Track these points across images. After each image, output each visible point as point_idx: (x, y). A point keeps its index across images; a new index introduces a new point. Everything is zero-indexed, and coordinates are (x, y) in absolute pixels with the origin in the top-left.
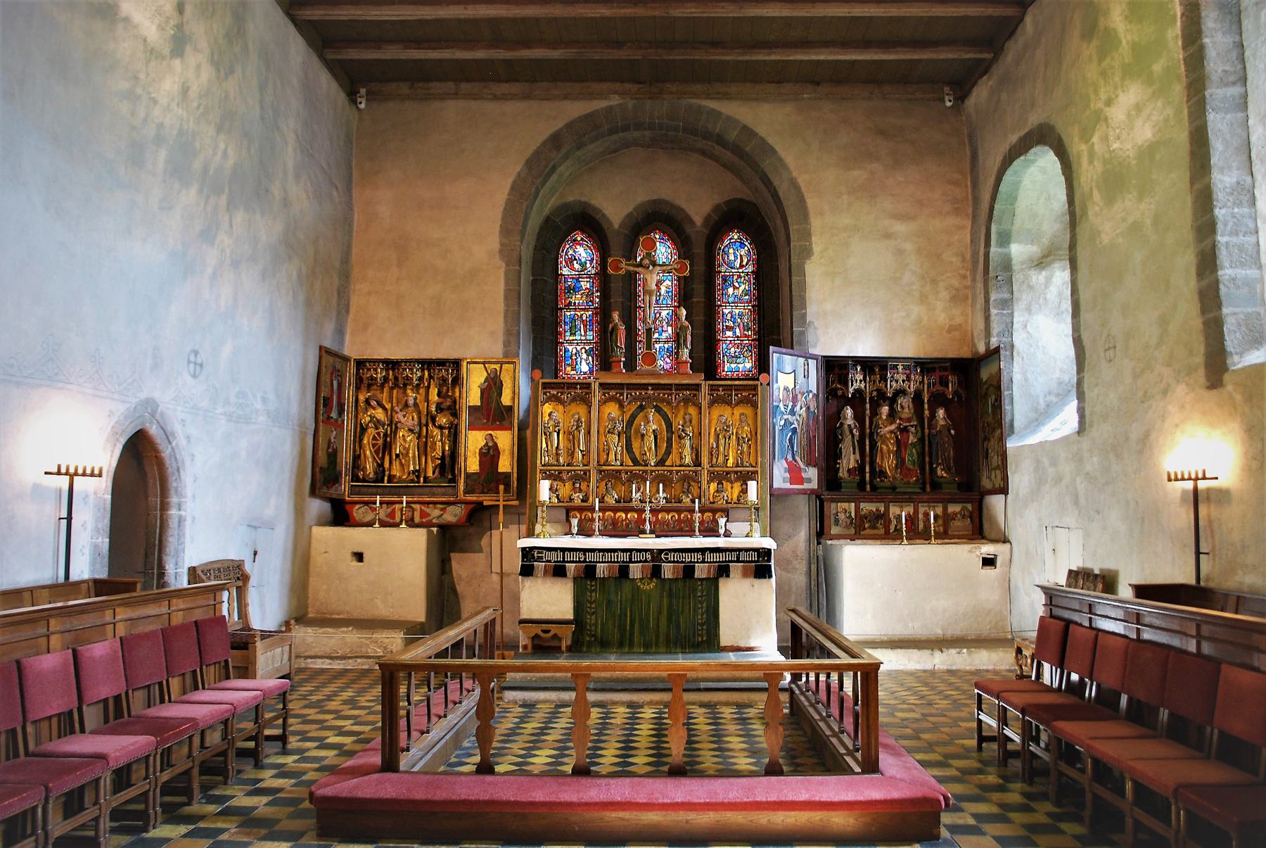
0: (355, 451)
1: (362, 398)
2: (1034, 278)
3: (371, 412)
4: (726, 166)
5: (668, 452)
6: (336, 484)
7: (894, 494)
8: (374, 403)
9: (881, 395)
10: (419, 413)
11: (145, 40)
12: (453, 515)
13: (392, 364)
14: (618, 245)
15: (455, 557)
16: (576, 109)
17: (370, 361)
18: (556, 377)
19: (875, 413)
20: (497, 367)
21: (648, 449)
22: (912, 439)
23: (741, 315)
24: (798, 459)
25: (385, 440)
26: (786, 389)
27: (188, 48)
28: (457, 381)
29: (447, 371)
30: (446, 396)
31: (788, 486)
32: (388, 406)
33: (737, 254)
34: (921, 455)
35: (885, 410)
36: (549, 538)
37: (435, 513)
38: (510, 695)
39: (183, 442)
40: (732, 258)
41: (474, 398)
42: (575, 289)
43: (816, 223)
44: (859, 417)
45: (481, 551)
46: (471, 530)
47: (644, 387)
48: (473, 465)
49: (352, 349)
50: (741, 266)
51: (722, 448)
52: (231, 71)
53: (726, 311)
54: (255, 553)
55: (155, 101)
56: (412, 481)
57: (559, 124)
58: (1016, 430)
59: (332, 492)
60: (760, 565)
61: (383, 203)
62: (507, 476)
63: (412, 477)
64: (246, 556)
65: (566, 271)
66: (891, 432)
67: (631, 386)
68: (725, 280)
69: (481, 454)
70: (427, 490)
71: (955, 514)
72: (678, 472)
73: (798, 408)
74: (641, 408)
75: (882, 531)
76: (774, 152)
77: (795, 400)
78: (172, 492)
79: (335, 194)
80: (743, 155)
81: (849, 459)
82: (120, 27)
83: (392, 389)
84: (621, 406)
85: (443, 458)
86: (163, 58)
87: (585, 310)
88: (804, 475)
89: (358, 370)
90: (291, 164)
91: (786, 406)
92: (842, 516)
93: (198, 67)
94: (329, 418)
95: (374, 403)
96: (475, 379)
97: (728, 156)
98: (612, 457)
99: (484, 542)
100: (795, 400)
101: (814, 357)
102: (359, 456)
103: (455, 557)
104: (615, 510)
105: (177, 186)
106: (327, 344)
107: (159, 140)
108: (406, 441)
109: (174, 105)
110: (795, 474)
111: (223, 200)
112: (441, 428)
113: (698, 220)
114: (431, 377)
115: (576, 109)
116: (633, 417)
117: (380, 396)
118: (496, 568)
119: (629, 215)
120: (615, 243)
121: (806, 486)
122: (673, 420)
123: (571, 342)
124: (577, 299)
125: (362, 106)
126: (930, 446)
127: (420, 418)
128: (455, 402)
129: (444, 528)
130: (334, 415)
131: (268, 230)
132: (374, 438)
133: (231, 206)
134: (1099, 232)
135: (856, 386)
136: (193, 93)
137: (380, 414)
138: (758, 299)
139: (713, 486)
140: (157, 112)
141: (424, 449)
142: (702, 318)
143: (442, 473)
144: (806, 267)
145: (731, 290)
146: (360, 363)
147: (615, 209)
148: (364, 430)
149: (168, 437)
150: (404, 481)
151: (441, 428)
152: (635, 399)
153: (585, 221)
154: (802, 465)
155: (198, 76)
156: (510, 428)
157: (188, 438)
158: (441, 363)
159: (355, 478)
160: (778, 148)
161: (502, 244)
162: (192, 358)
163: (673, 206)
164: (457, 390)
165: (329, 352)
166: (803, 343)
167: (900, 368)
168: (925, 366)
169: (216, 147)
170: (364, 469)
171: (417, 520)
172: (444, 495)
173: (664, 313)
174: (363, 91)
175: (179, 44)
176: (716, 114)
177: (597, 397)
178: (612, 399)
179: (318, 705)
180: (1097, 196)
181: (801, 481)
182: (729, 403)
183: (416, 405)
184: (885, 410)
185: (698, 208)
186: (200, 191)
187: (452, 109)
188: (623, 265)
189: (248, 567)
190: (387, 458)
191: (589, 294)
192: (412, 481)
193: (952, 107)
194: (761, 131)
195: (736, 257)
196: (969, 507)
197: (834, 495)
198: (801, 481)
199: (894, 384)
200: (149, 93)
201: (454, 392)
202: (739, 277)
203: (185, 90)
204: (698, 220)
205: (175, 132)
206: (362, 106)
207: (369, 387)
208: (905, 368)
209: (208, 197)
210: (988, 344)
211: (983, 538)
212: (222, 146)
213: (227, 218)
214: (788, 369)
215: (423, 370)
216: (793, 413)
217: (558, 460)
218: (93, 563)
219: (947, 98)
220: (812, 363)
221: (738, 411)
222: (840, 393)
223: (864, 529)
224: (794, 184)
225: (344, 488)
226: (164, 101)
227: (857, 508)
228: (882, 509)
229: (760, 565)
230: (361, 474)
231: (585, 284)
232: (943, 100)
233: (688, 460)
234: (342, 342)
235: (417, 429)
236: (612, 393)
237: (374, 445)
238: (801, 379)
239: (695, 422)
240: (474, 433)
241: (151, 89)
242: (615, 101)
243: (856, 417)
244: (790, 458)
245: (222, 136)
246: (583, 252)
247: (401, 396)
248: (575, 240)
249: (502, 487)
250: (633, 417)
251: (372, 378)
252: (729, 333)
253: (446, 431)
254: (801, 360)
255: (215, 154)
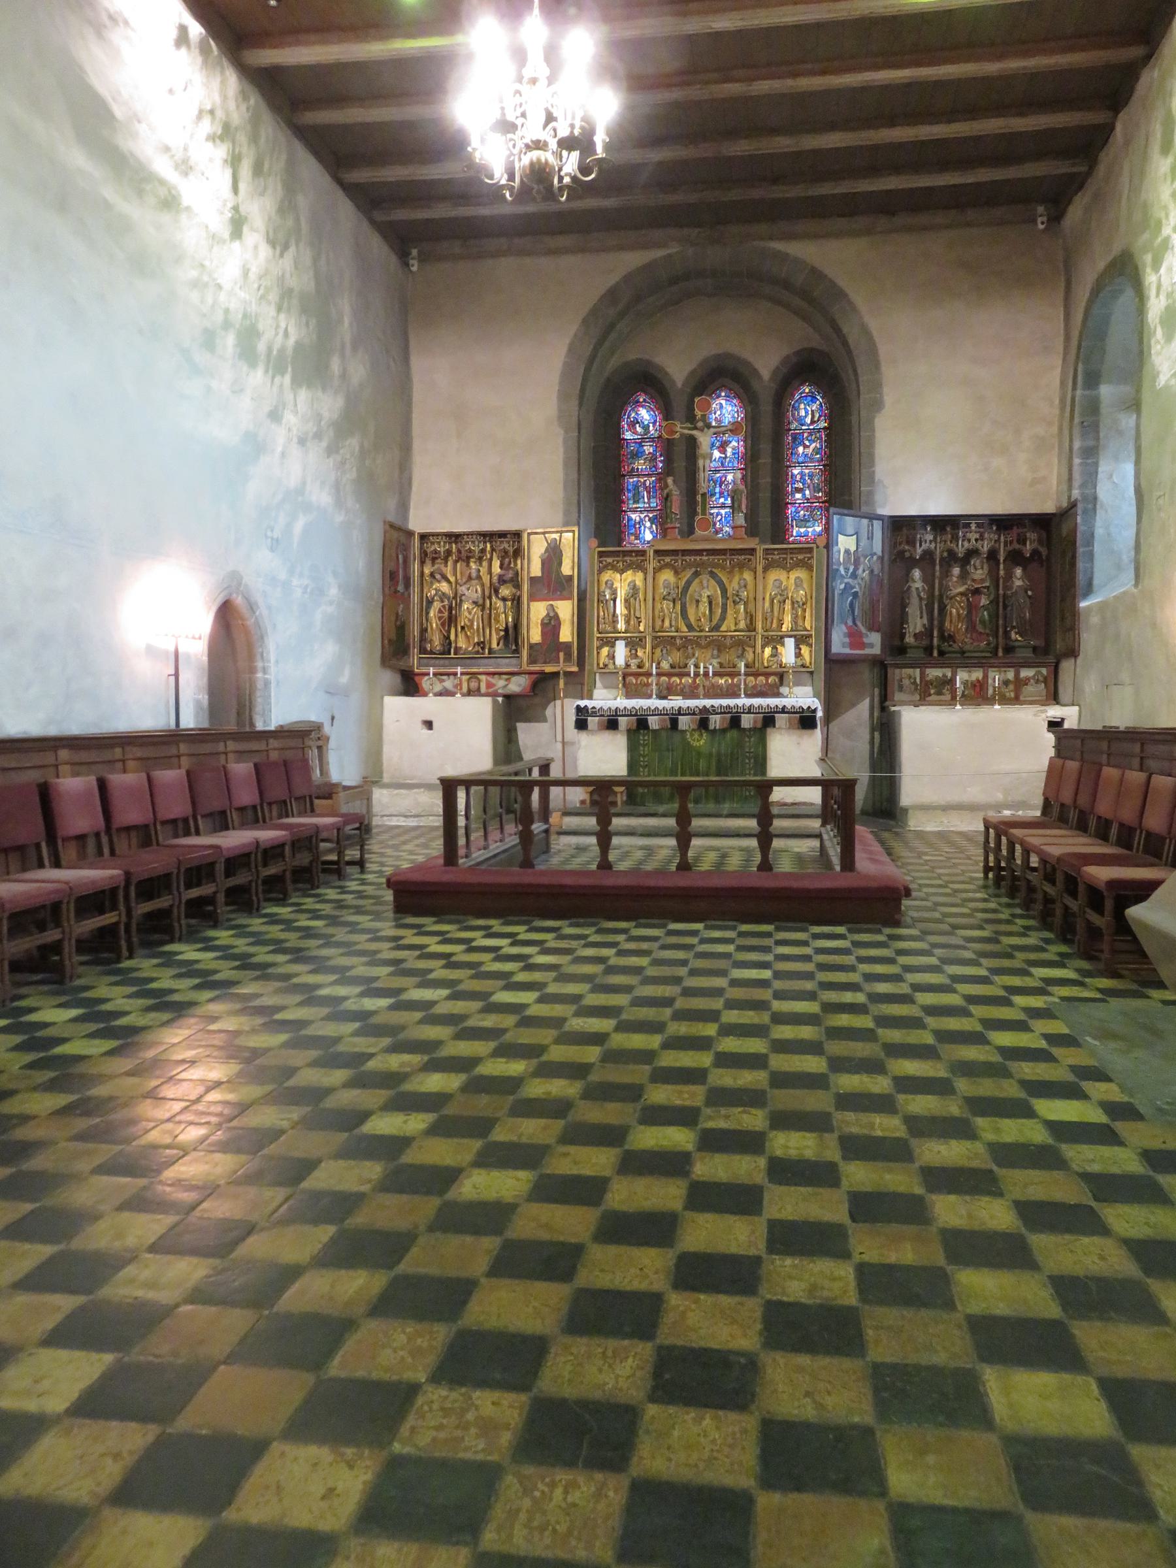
0: (422, 624)
1: (427, 571)
2: (1124, 423)
3: (436, 585)
4: (796, 312)
5: (723, 618)
6: (403, 654)
7: (966, 660)
8: (438, 576)
9: (952, 554)
10: (483, 585)
11: (207, 227)
12: (517, 685)
13: (455, 537)
14: (681, 405)
15: (520, 726)
16: (634, 259)
17: (433, 535)
18: (619, 545)
19: (946, 574)
20: (556, 536)
21: (699, 612)
22: (984, 601)
23: (811, 476)
24: (859, 624)
25: (450, 612)
26: (847, 552)
27: (245, 229)
28: (518, 553)
29: (510, 543)
30: (509, 568)
31: (847, 651)
32: (452, 579)
33: (808, 411)
34: (994, 616)
35: (956, 571)
36: (605, 698)
37: (500, 683)
38: (565, 840)
39: (265, 612)
40: (803, 413)
41: (536, 570)
42: (636, 455)
43: (889, 373)
44: (928, 579)
45: (545, 720)
46: (537, 700)
47: (699, 552)
48: (536, 636)
49: (418, 523)
50: (813, 422)
51: (776, 614)
52: (286, 247)
53: (796, 472)
54: (333, 718)
55: (219, 287)
56: (478, 653)
57: (613, 279)
58: (1095, 588)
59: (402, 664)
60: (806, 721)
61: (436, 372)
62: (567, 646)
63: (477, 648)
64: (324, 719)
65: (628, 435)
66: (962, 594)
67: (685, 552)
68: (794, 439)
69: (543, 624)
70: (493, 660)
71: (1028, 679)
72: (732, 637)
73: (860, 571)
74: (696, 574)
75: (948, 697)
76: (846, 295)
77: (857, 563)
78: (258, 657)
79: (392, 364)
80: (815, 300)
81: (916, 622)
82: (184, 217)
83: (456, 562)
84: (676, 573)
85: (506, 630)
86: (224, 242)
87: (649, 475)
88: (865, 640)
89: (422, 544)
90: (348, 339)
91: (847, 569)
92: (906, 682)
93: (256, 247)
94: (396, 592)
95: (438, 576)
96: (537, 549)
97: (797, 301)
98: (667, 623)
99: (549, 712)
100: (857, 563)
101: (880, 518)
102: (426, 630)
103: (520, 726)
104: (669, 675)
105: (245, 368)
106: (391, 518)
107: (227, 325)
108: (468, 611)
109: (237, 289)
110: (855, 638)
111: (287, 379)
112: (504, 599)
113: (766, 374)
114: (493, 550)
115: (634, 259)
116: (688, 584)
117: (444, 569)
118: (559, 738)
119: (693, 373)
120: (679, 404)
121: (867, 651)
122: (727, 586)
123: (634, 511)
124: (641, 465)
125: (414, 269)
126: (1005, 607)
127: (483, 591)
128: (517, 573)
129: (507, 697)
130: (400, 588)
131: (331, 405)
132: (440, 611)
133: (296, 383)
134: (1158, 373)
135: (925, 546)
136: (252, 276)
137: (444, 587)
138: (829, 457)
139: (768, 651)
140: (222, 297)
141: (488, 621)
142: (769, 480)
143: (506, 644)
144: (876, 420)
145: (801, 449)
146: (424, 537)
147: (678, 368)
148: (430, 602)
149: (252, 607)
150: (470, 653)
151: (504, 599)
152: (690, 565)
153: (646, 381)
154: (863, 630)
155: (256, 256)
156: (570, 598)
157: (269, 608)
158: (502, 535)
159: (423, 650)
160: (848, 291)
161: (560, 410)
162: (269, 534)
163: (738, 359)
164: (519, 562)
165: (392, 526)
166: (870, 502)
167: (973, 527)
168: (1002, 523)
169: (278, 327)
170: (431, 641)
171: (483, 690)
172: (508, 665)
173: (730, 477)
174: (415, 252)
175: (238, 225)
176: (784, 257)
177: (651, 565)
178: (667, 566)
179: (394, 847)
180: (1159, 333)
181: (862, 646)
182: (784, 568)
183: (479, 577)
184: (956, 571)
185: (766, 363)
186: (266, 371)
187: (506, 265)
188: (678, 429)
189: (327, 729)
190: (453, 631)
191: (652, 459)
192: (478, 653)
193: (1045, 228)
194: (831, 272)
195: (807, 412)
196: (1044, 671)
197: (899, 660)
198: (862, 646)
199: (966, 544)
200: (214, 280)
201: (516, 564)
202: (810, 434)
203: (246, 273)
204: (766, 374)
205: (240, 316)
206: (414, 269)
207: (434, 560)
208: (978, 526)
209: (273, 378)
210: (1069, 497)
211: (1058, 703)
212: (283, 325)
213: (291, 396)
214: (850, 530)
215: (485, 542)
216: (854, 576)
217: (615, 627)
218: (197, 715)
219: (1039, 220)
220: (877, 525)
221: (794, 575)
222: (907, 555)
223: (926, 693)
224: (865, 331)
225: (414, 660)
226: (227, 286)
227: (922, 675)
228: (949, 675)
229: (806, 721)
230: (428, 647)
231: (648, 449)
232: (1034, 221)
233: (742, 625)
234: (405, 517)
235: (481, 602)
236: (668, 559)
237: (440, 618)
238: (864, 542)
239: (750, 586)
240: (536, 604)
241: (216, 276)
242: (673, 249)
243: (924, 580)
244: (850, 623)
245: (282, 316)
246: (644, 414)
247: (465, 568)
248: (638, 402)
249: (561, 655)
250: (688, 584)
251: (435, 552)
252: (798, 496)
253: (509, 603)
254: (865, 522)
255: (277, 334)
